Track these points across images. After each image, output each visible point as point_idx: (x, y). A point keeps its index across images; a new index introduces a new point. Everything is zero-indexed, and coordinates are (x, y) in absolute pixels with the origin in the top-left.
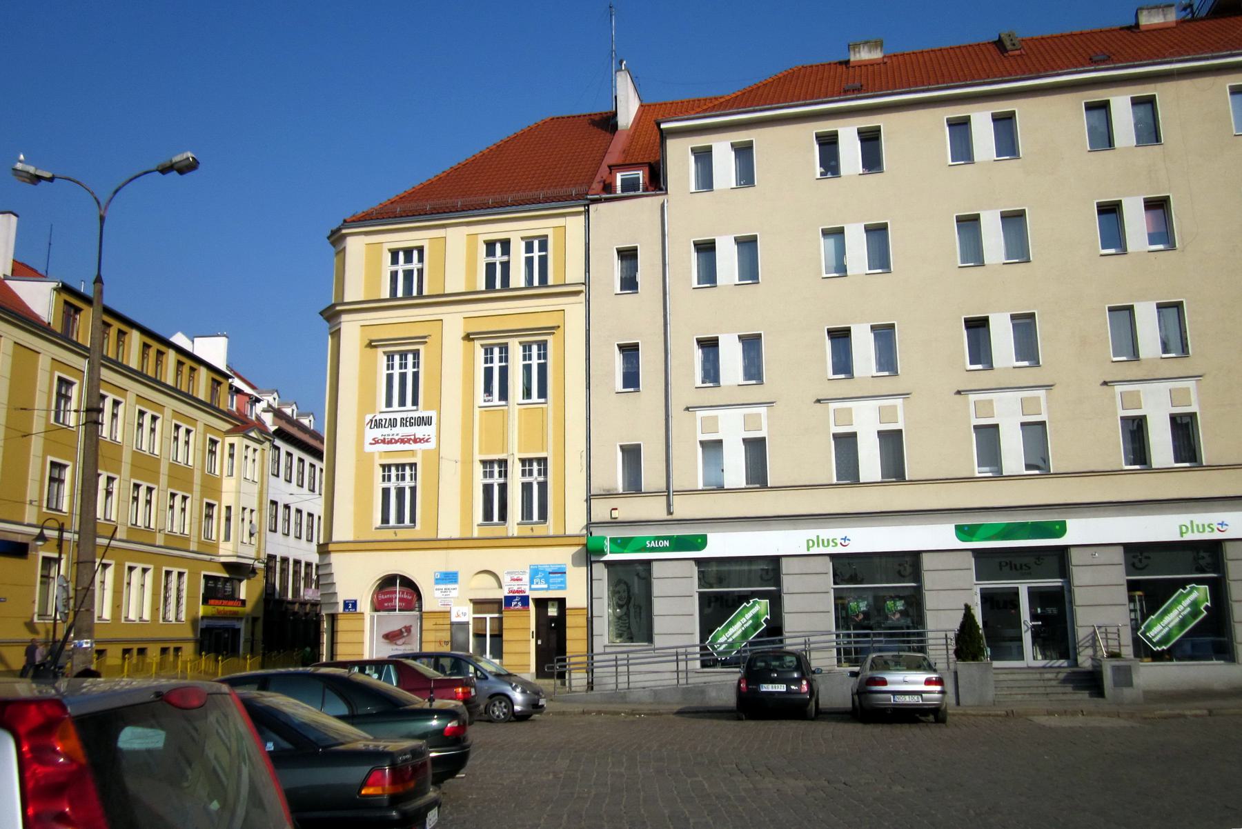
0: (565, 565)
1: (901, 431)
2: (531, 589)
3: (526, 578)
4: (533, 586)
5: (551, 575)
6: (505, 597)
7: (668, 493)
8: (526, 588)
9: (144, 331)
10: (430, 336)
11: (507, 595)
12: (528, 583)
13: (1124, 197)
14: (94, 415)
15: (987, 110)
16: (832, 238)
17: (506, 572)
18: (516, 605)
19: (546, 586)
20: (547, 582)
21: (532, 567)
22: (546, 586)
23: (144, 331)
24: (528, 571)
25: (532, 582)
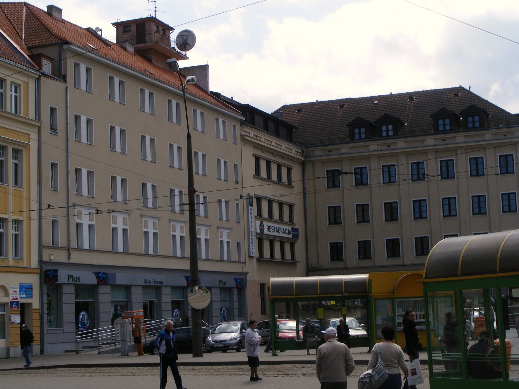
0: (32, 284)
1: (157, 233)
2: (21, 298)
3: (18, 290)
4: (21, 296)
5: (28, 290)
6: (11, 302)
7: (69, 249)
8: (18, 297)
9: (225, 261)
10: (211, 226)
11: (11, 300)
12: (19, 294)
13: (83, 115)
14: (77, 328)
15: (149, 90)
16: (271, 163)
17: (10, 287)
18: (15, 307)
19: (25, 296)
20: (26, 294)
21: (20, 284)
22: (25, 296)
23: (225, 261)
24: (19, 287)
25: (20, 294)
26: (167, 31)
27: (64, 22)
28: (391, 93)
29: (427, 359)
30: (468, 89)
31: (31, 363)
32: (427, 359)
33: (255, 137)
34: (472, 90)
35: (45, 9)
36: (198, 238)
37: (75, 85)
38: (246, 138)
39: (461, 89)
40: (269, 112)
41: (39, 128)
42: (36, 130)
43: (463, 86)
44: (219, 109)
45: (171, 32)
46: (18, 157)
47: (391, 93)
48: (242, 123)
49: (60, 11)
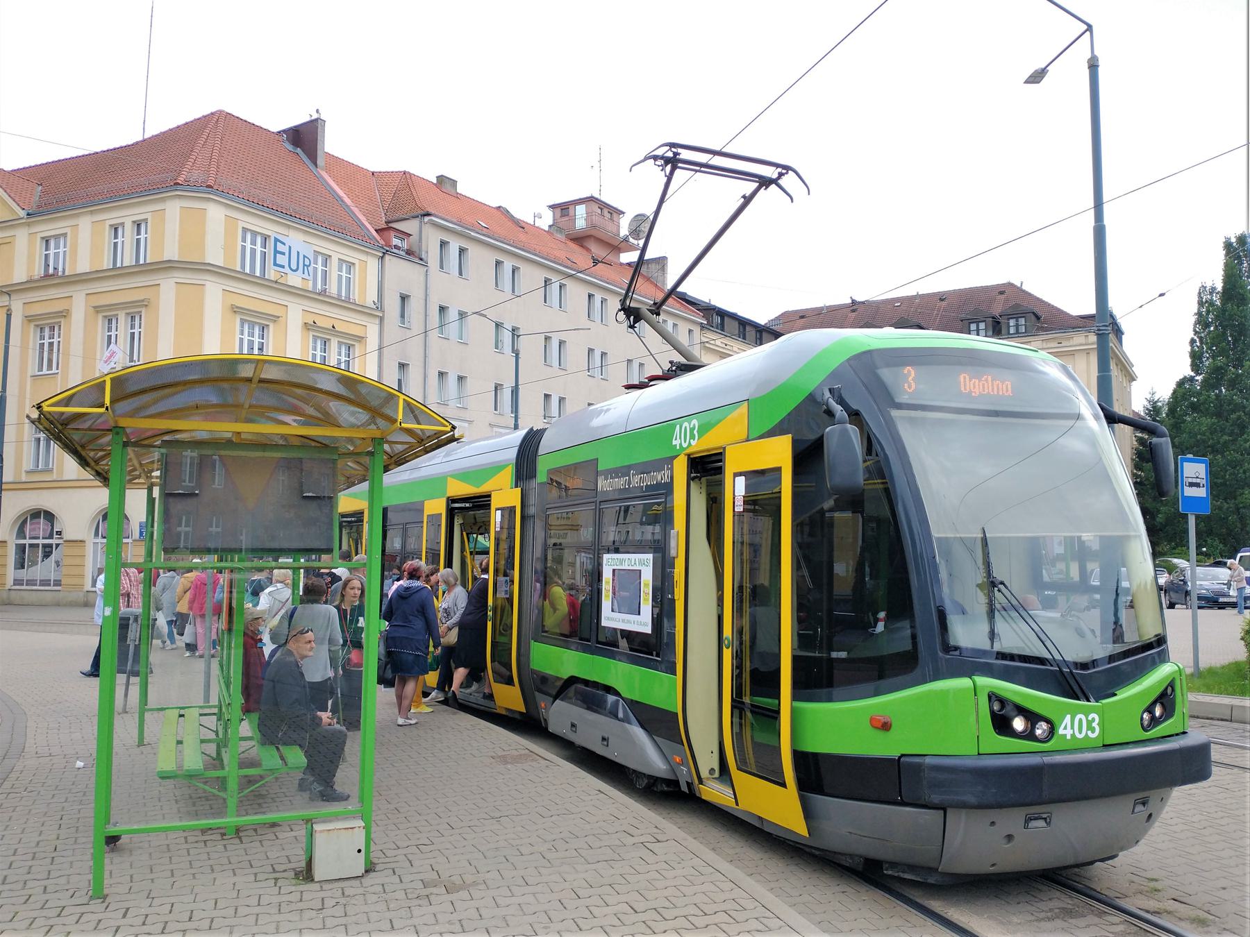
26: (615, 215)
27: (458, 196)
28: (918, 293)
29: (650, 632)
30: (1019, 285)
31: (1234, 673)
32: (650, 632)
33: (724, 346)
34: (1024, 288)
35: (435, 181)
36: (939, 539)
37: (602, 321)
38: (707, 345)
39: (1010, 285)
40: (763, 323)
41: (382, 319)
42: (377, 321)
43: (1012, 281)
44: (546, 262)
45: (621, 216)
46: (325, 349)
47: (918, 293)
48: (702, 327)
49: (454, 182)
